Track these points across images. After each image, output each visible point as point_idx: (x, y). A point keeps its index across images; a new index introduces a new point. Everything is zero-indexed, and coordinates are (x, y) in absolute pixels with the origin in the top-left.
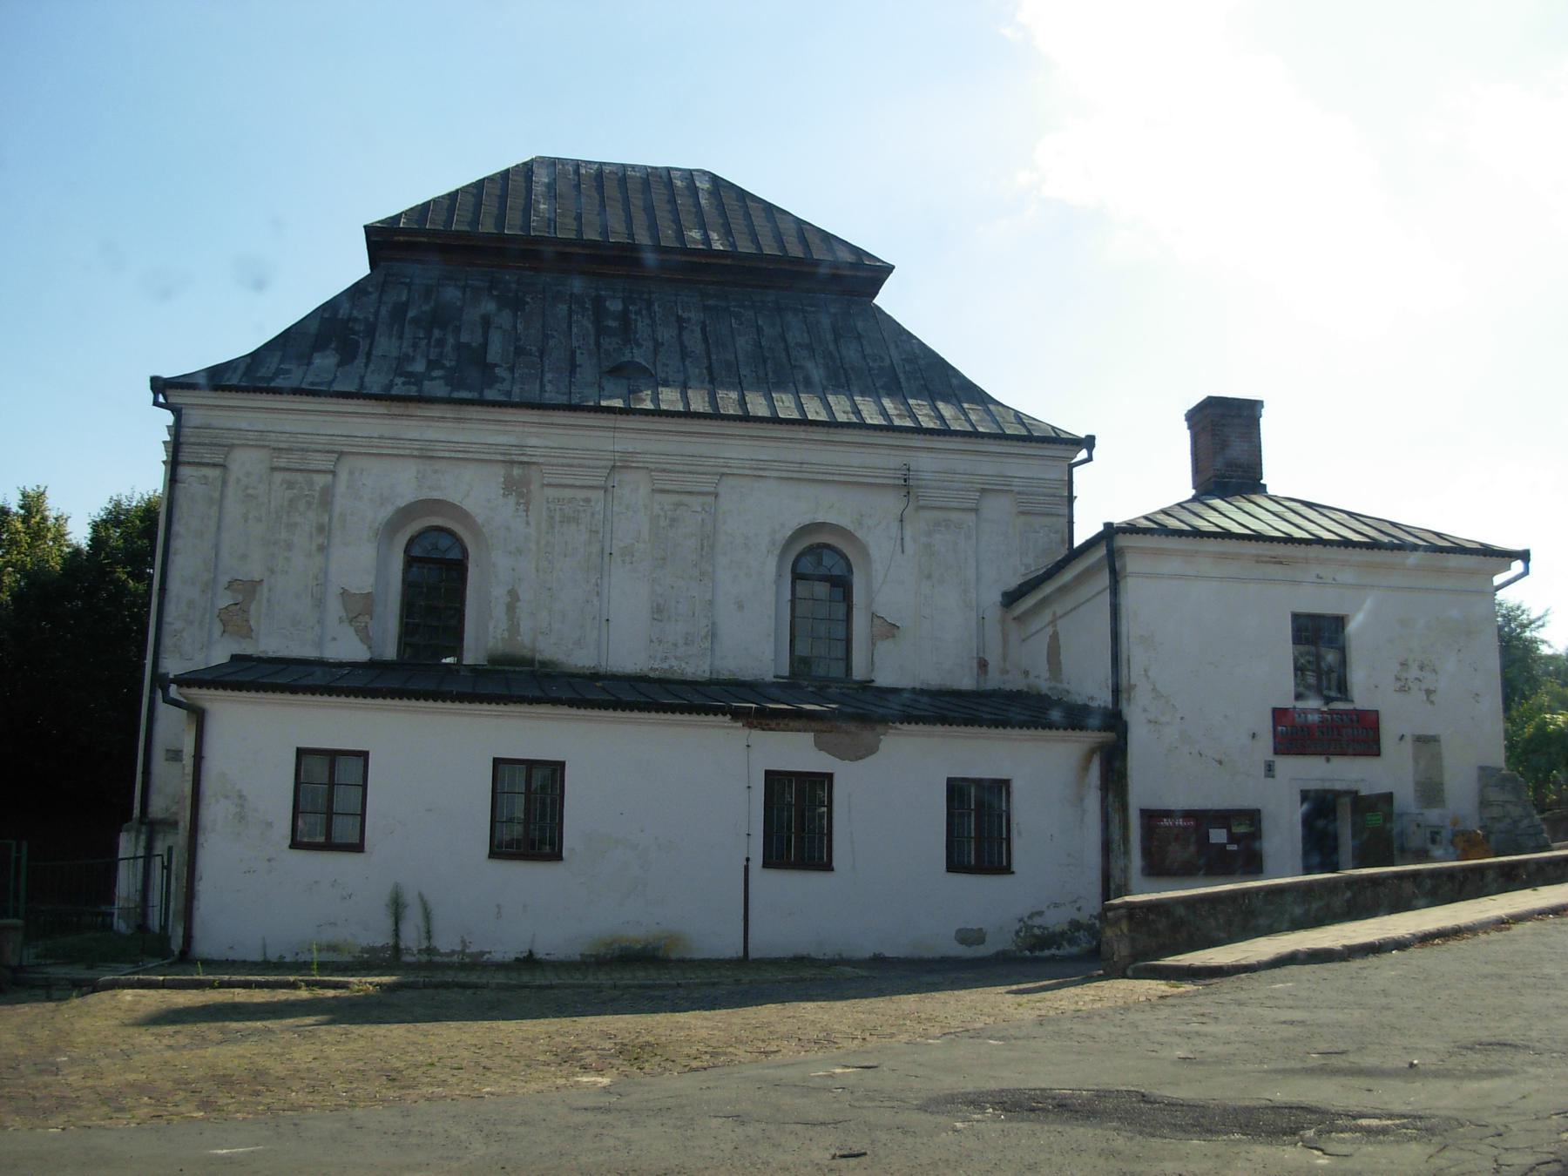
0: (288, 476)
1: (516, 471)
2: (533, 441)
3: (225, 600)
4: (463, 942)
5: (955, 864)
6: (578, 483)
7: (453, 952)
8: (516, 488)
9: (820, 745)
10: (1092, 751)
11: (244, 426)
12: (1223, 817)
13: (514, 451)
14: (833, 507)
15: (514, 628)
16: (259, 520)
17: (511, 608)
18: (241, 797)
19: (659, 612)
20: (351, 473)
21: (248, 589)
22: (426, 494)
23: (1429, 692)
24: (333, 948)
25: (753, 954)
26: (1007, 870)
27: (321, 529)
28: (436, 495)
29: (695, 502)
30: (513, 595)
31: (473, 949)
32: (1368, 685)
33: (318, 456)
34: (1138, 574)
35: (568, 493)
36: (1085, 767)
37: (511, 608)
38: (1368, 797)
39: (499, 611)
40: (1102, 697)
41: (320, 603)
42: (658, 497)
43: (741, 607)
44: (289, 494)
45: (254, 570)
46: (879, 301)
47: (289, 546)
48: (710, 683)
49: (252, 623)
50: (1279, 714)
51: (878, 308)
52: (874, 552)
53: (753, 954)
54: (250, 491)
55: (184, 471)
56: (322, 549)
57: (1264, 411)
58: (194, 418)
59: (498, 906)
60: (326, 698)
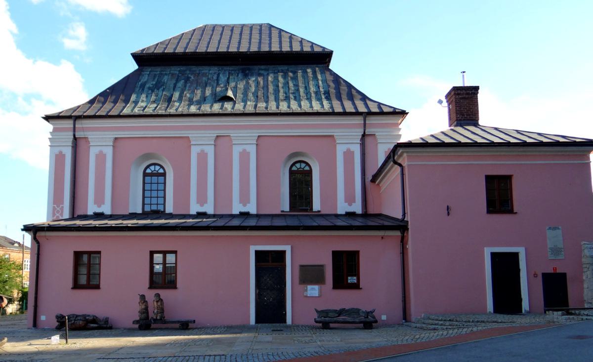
57: (479, 91)
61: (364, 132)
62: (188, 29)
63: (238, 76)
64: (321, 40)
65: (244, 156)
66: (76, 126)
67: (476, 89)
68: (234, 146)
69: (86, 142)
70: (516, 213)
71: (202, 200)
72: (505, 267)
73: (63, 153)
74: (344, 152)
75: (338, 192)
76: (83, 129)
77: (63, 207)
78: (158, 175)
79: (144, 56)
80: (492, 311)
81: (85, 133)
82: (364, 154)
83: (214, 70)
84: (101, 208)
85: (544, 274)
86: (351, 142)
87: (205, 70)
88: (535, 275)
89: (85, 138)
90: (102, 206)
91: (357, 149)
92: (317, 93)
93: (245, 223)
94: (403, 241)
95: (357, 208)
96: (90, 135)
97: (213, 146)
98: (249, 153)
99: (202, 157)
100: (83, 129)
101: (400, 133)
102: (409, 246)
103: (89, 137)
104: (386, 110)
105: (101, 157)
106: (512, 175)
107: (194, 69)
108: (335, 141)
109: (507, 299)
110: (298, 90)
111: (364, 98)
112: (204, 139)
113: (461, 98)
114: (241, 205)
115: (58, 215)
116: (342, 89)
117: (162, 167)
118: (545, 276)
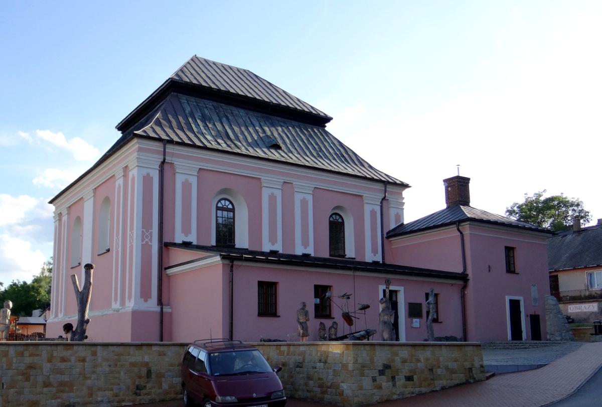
57: (470, 181)
61: (164, 159)
62: (188, 59)
63: (266, 123)
64: (321, 106)
65: (304, 202)
66: (167, 150)
67: (468, 179)
68: (263, 188)
69: (171, 167)
70: (518, 274)
71: (273, 240)
72: (515, 305)
73: (151, 176)
74: (371, 211)
75: (363, 244)
76: (173, 155)
77: (151, 232)
78: (228, 210)
79: (182, 83)
80: (511, 339)
81: (173, 159)
82: (162, 223)
83: (242, 112)
84: (306, 250)
85: (530, 315)
86: (373, 203)
87: (236, 111)
88: (527, 316)
89: (171, 163)
90: (275, 244)
91: (378, 209)
92: (336, 154)
93: (304, 261)
94: (465, 287)
95: (379, 258)
96: (177, 162)
97: (312, 195)
98: (191, 184)
99: (272, 198)
100: (173, 155)
101: (404, 201)
102: (470, 292)
103: (175, 163)
104: (398, 182)
105: (187, 186)
106: (515, 248)
107: (225, 107)
108: (261, 183)
109: (517, 333)
110: (321, 149)
111: (370, 167)
112: (275, 182)
113: (461, 185)
114: (303, 247)
115: (147, 240)
116: (345, 154)
117: (231, 202)
118: (531, 316)
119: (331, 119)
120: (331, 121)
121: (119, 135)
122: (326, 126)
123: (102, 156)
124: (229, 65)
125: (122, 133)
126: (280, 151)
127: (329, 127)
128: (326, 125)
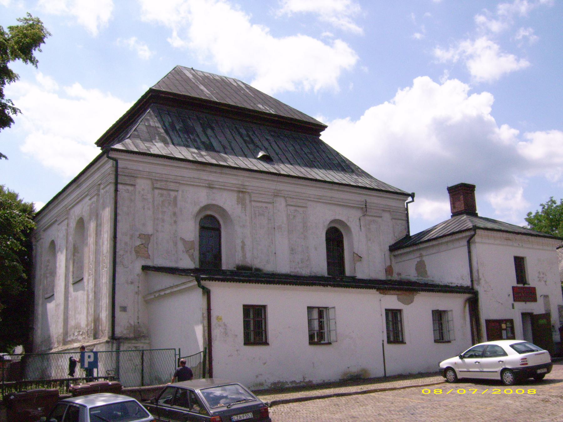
0: (160, 191)
1: (241, 195)
2: (247, 184)
3: (138, 243)
4: (304, 377)
5: (247, 342)
6: (263, 200)
7: (301, 382)
8: (241, 202)
9: (399, 299)
10: (466, 301)
11: (141, 169)
12: (506, 321)
13: (241, 187)
14: (341, 214)
15: (244, 256)
16: (149, 209)
17: (243, 248)
18: (225, 325)
19: (292, 250)
20: (183, 192)
21: (146, 238)
22: (210, 202)
23: (545, 282)
24: (261, 384)
25: (387, 375)
26: (266, 343)
27: (175, 214)
28: (214, 202)
29: (301, 210)
30: (243, 242)
31: (307, 380)
32: (532, 280)
33: (172, 184)
34: (478, 242)
35: (260, 204)
36: (465, 306)
37: (243, 248)
38: (536, 315)
39: (239, 249)
40: (467, 283)
41: (176, 244)
42: (288, 207)
43: (316, 249)
44: (161, 199)
45: (149, 230)
46: (321, 138)
47: (163, 221)
48: (310, 277)
49: (149, 252)
50: (514, 288)
51: (321, 141)
52: (353, 230)
53: (387, 375)
54: (145, 197)
55: (120, 187)
56: (175, 222)
57: (476, 189)
58: (121, 164)
59: (313, 363)
60: (248, 284)
119: (326, 127)
120: (326, 129)
121: (98, 151)
122: (320, 135)
123: (114, 122)
124: (233, 78)
125: (101, 149)
126: (271, 194)
127: (324, 137)
128: (321, 133)
